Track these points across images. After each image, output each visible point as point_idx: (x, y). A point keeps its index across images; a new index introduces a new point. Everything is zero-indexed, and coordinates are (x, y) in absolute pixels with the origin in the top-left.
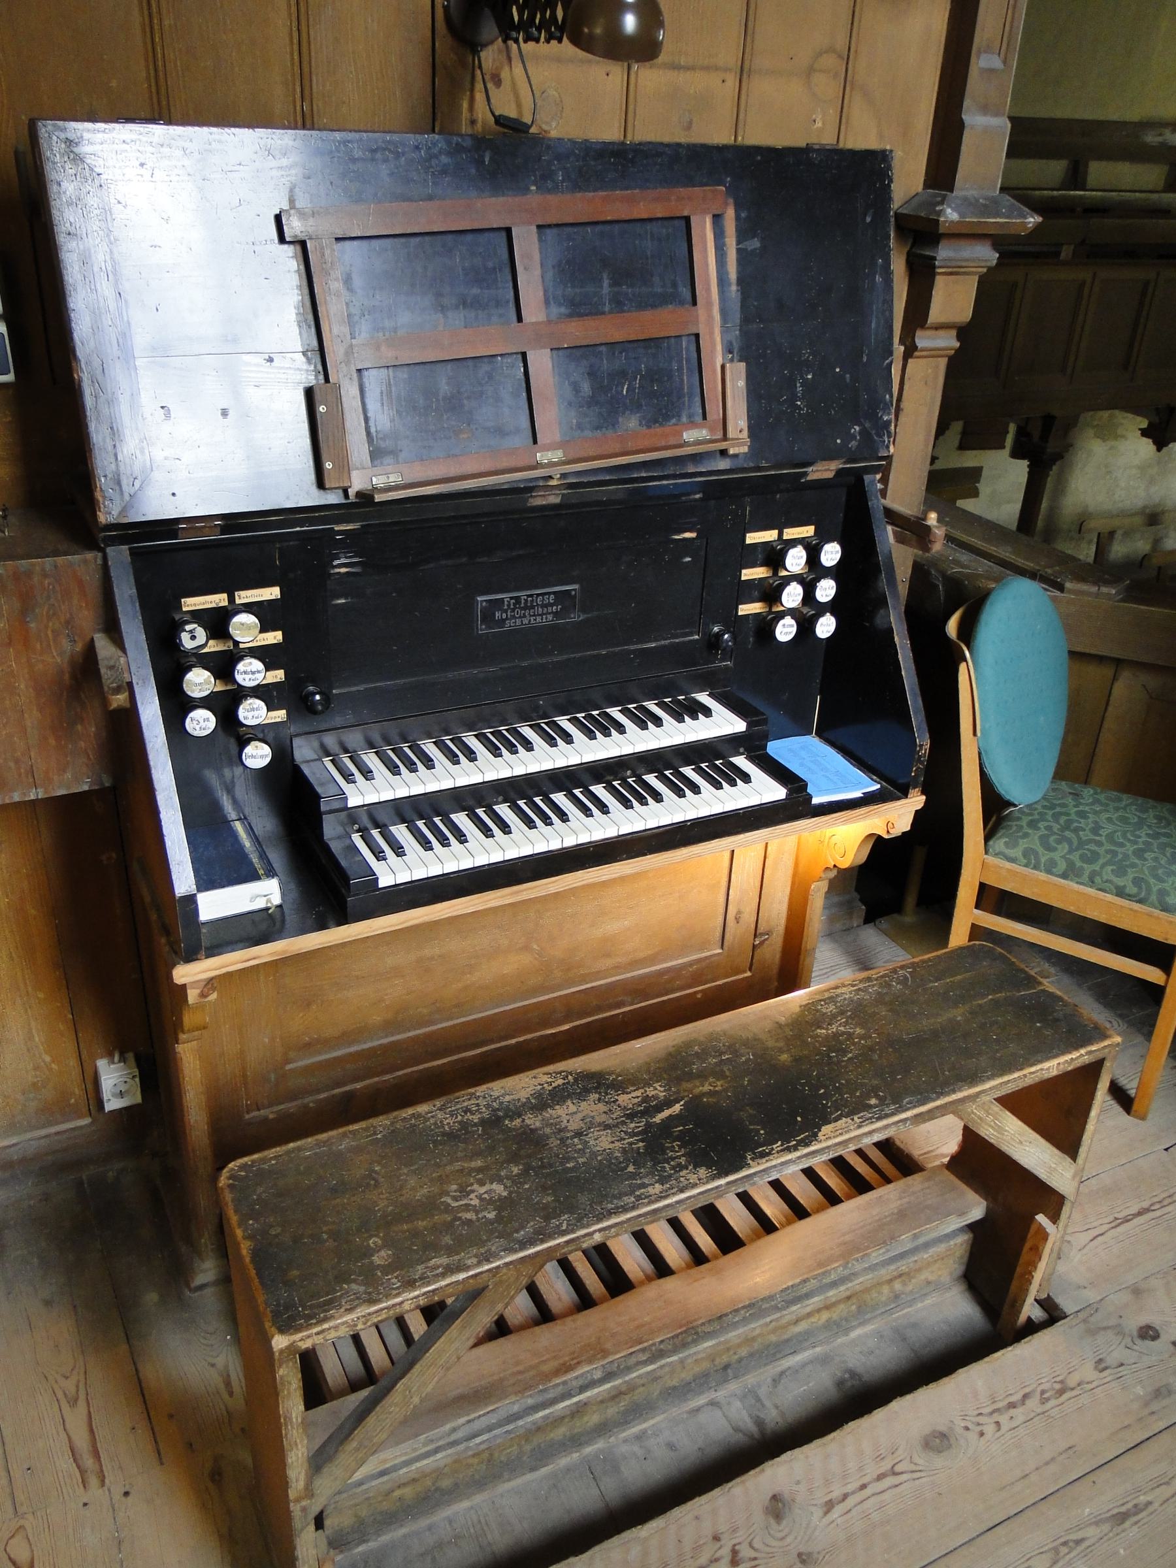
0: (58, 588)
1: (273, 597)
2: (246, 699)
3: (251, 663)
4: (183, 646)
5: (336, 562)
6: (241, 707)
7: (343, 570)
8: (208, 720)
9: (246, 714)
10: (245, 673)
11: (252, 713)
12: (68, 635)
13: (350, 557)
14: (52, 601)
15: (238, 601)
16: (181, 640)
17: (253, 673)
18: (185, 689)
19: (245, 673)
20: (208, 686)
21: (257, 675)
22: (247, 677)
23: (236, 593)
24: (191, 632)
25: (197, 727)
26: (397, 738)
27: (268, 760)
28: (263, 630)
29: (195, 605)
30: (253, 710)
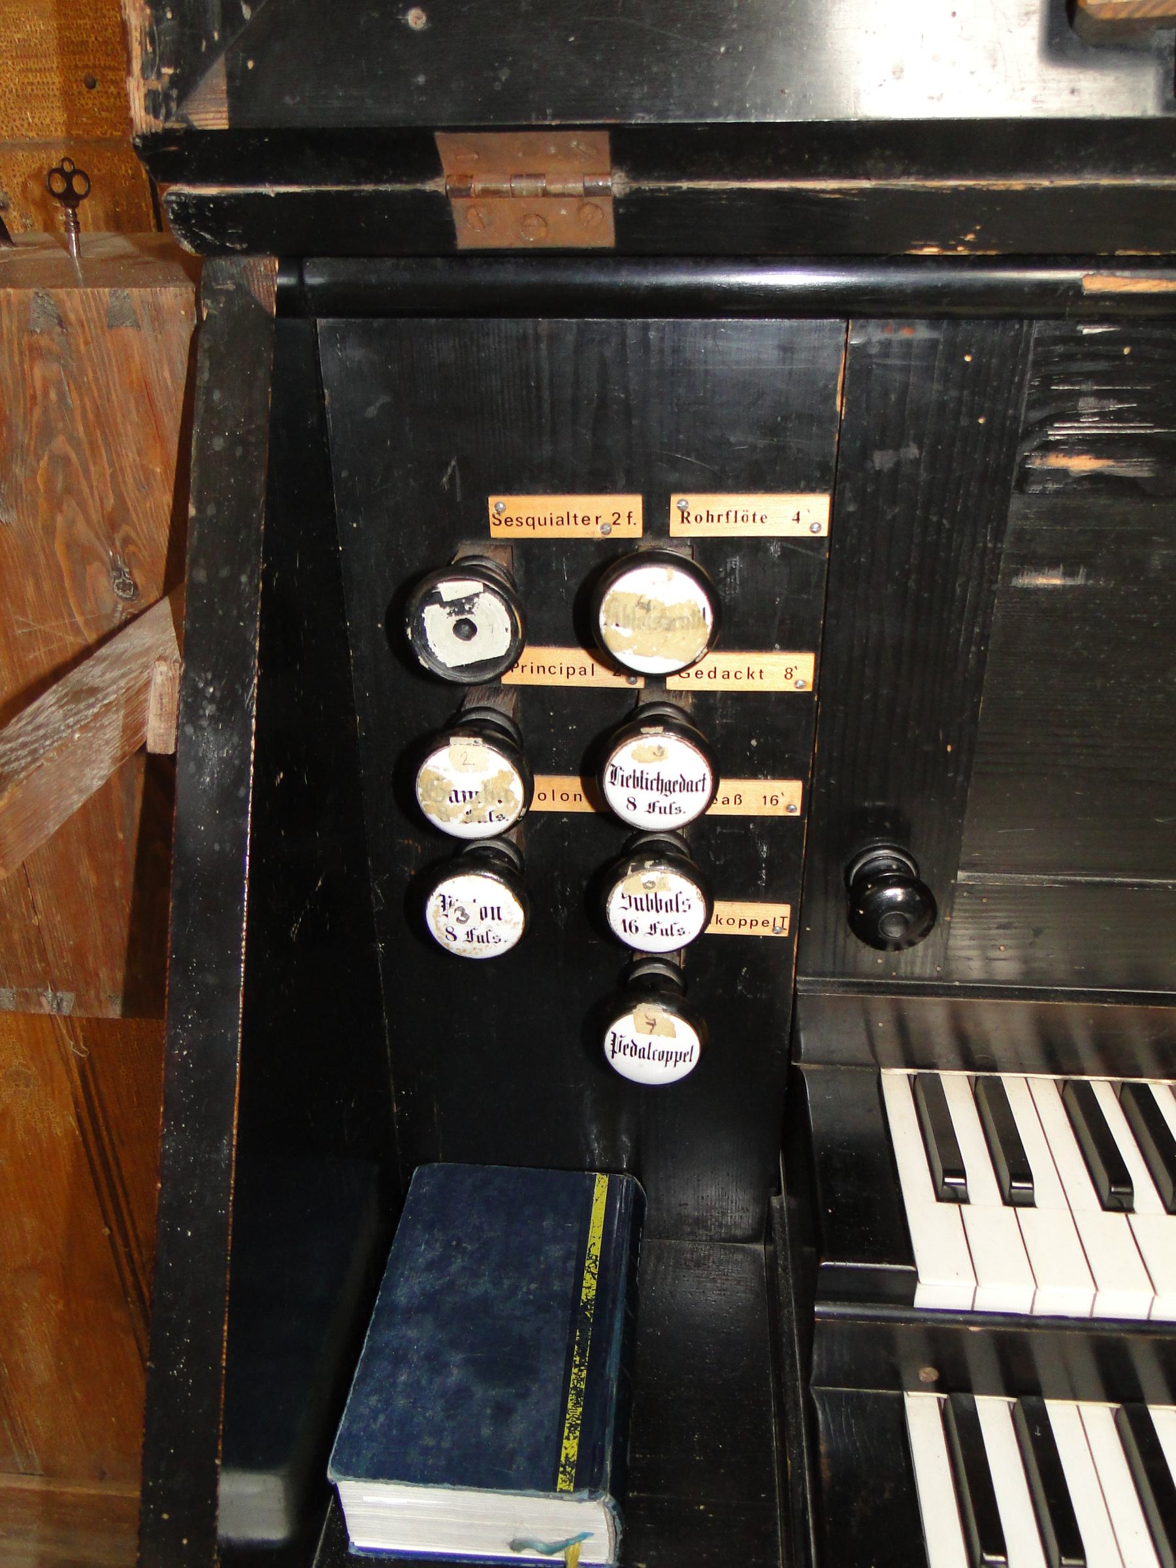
0: (73, 400)
1: (801, 530)
2: (639, 868)
3: (660, 752)
4: (431, 654)
5: (1059, 432)
6: (619, 889)
7: (1082, 464)
8: (496, 913)
9: (631, 915)
10: (638, 781)
11: (650, 917)
12: (115, 568)
13: (1119, 416)
14: (60, 444)
15: (677, 529)
16: (421, 632)
17: (666, 787)
18: (424, 803)
19: (638, 781)
20: (495, 807)
21: (679, 798)
22: (644, 797)
23: (675, 499)
24: (458, 606)
25: (461, 931)
26: (1144, 1057)
27: (684, 1068)
28: (721, 640)
29: (532, 522)
30: (656, 905)
